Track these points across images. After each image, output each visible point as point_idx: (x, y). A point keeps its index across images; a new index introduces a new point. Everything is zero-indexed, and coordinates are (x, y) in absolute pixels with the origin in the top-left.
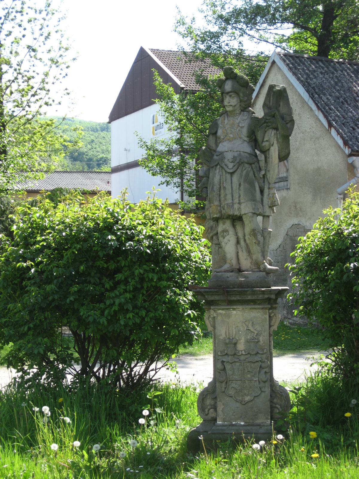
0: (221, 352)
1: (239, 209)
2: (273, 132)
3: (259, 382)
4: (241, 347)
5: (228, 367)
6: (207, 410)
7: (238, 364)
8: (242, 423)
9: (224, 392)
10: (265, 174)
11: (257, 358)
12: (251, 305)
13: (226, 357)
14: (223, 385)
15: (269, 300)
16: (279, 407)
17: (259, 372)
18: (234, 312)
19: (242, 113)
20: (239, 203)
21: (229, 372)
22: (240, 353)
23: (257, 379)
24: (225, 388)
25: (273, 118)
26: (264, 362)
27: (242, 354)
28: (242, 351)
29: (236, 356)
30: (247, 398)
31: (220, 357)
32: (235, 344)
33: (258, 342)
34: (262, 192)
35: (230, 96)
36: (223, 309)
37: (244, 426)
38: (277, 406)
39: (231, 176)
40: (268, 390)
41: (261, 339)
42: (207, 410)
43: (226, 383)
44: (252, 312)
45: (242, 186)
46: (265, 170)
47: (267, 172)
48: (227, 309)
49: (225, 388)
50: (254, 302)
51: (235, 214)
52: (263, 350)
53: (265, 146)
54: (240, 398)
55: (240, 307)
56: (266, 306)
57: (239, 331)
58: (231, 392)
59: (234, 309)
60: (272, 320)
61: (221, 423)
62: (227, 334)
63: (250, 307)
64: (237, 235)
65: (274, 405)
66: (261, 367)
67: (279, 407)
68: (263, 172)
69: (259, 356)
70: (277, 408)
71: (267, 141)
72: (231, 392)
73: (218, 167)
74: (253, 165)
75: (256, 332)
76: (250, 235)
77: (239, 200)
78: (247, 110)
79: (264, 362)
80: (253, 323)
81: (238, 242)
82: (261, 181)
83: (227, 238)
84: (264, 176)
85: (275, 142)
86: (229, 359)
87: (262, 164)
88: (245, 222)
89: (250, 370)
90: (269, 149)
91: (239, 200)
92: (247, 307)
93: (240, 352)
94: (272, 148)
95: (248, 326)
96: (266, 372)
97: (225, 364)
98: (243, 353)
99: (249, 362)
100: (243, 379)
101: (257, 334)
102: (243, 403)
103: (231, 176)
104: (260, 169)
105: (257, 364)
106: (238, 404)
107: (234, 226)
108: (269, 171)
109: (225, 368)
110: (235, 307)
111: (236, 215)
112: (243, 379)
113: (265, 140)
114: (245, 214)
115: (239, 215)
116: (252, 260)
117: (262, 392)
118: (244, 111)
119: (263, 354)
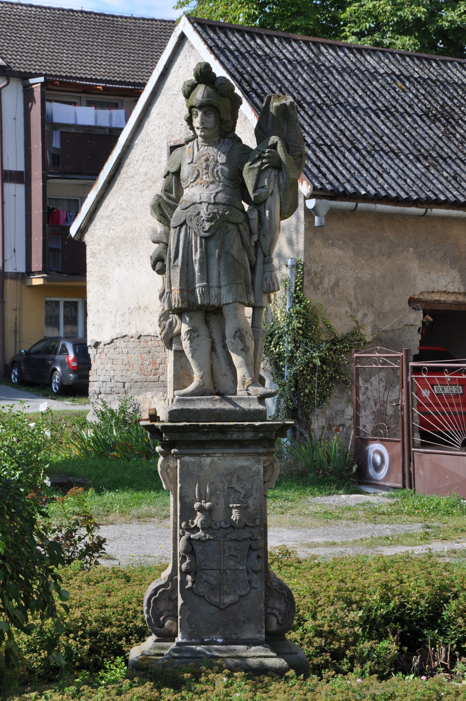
1: (218, 296)
2: (273, 174)
3: (248, 572)
10: (258, 241)
11: (246, 534)
12: (235, 448)
16: (277, 613)
17: (248, 556)
18: (209, 460)
19: (222, 140)
20: (219, 287)
22: (218, 525)
23: (244, 567)
26: (255, 540)
27: (221, 527)
28: (220, 522)
30: (228, 600)
34: (253, 269)
38: (275, 611)
40: (259, 585)
44: (237, 460)
46: (259, 234)
47: (261, 237)
48: (198, 455)
51: (212, 303)
52: (254, 521)
54: (217, 600)
55: (218, 452)
56: (261, 451)
57: (216, 490)
59: (208, 455)
66: (250, 548)
67: (277, 613)
68: (255, 238)
69: (248, 529)
70: (274, 615)
75: (243, 492)
76: (235, 337)
77: (219, 282)
78: (230, 136)
79: (255, 540)
81: (213, 349)
82: (252, 252)
84: (257, 243)
85: (276, 190)
87: (254, 224)
88: (226, 316)
90: (265, 201)
91: (219, 282)
92: (230, 451)
93: (218, 524)
95: (230, 483)
96: (258, 557)
98: (223, 524)
99: (232, 540)
104: (251, 233)
107: (207, 323)
108: (264, 236)
109: (193, 549)
110: (210, 451)
111: (213, 306)
114: (227, 304)
115: (217, 305)
116: (66, 480)
117: (252, 588)
118: (224, 138)
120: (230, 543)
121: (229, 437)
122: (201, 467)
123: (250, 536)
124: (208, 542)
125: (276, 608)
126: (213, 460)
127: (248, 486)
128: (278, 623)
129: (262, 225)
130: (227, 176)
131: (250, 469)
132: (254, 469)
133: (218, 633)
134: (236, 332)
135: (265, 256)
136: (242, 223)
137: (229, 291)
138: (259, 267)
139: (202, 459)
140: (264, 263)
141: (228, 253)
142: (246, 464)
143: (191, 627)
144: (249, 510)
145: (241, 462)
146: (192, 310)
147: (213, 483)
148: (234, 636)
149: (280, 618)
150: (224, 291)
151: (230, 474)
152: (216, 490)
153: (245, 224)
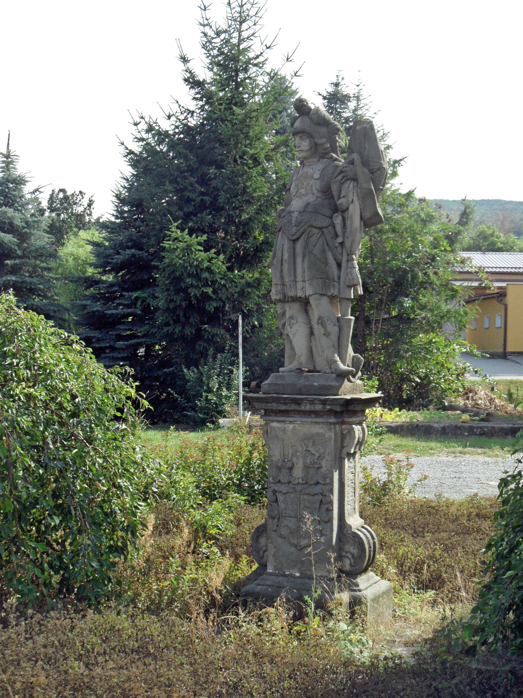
0: (273, 479)
2: (351, 185)
4: (298, 472)
5: (280, 497)
6: (261, 552)
7: (292, 495)
8: (297, 575)
9: (276, 531)
13: (279, 485)
14: (276, 521)
15: (336, 414)
18: (291, 426)
21: (282, 506)
22: (296, 482)
24: (278, 526)
25: (352, 166)
27: (299, 483)
29: (291, 485)
31: (272, 485)
32: (291, 469)
33: (319, 468)
34: (339, 265)
35: (301, 138)
36: (278, 421)
37: (299, 577)
39: (294, 243)
41: (323, 463)
42: (261, 552)
43: (279, 519)
45: (307, 257)
47: (346, 239)
48: (283, 422)
49: (278, 526)
50: (317, 414)
52: (325, 479)
53: (341, 203)
54: (295, 542)
55: (299, 420)
57: (297, 451)
58: (284, 532)
59: (291, 422)
60: (345, 438)
61: (271, 571)
62: (282, 454)
63: (309, 420)
64: (310, 323)
65: (344, 554)
66: (321, 502)
67: (350, 556)
70: (348, 557)
71: (344, 197)
72: (284, 532)
73: (281, 232)
74: (325, 230)
75: (317, 455)
78: (327, 156)
80: (313, 442)
83: (295, 327)
85: (356, 199)
86: (284, 488)
89: (307, 504)
90: (348, 208)
94: (351, 207)
95: (307, 446)
97: (277, 494)
100: (299, 517)
101: (319, 457)
102: (299, 548)
103: (294, 243)
104: (337, 236)
105: (316, 497)
106: (293, 549)
108: (347, 237)
109: (277, 499)
110: (291, 419)
112: (299, 517)
113: (342, 196)
119: (324, 485)
120: (305, 497)
121: (303, 408)
122: (284, 430)
123: (321, 492)
124: (288, 494)
125: (350, 552)
126: (294, 427)
127: (322, 450)
128: (351, 564)
129: (346, 229)
130: (318, 188)
131: (324, 436)
132: (327, 436)
133: (296, 569)
134: (319, 319)
135: (348, 255)
136: (326, 227)
137: (311, 284)
138: (344, 265)
139: (286, 426)
140: (348, 261)
141: (311, 252)
142: (321, 431)
143: (275, 562)
144: (322, 470)
145: (317, 429)
146: (288, 301)
147: (294, 446)
148: (308, 572)
149: (352, 561)
150: (307, 285)
151: (310, 438)
152: (297, 451)
153: (330, 228)
